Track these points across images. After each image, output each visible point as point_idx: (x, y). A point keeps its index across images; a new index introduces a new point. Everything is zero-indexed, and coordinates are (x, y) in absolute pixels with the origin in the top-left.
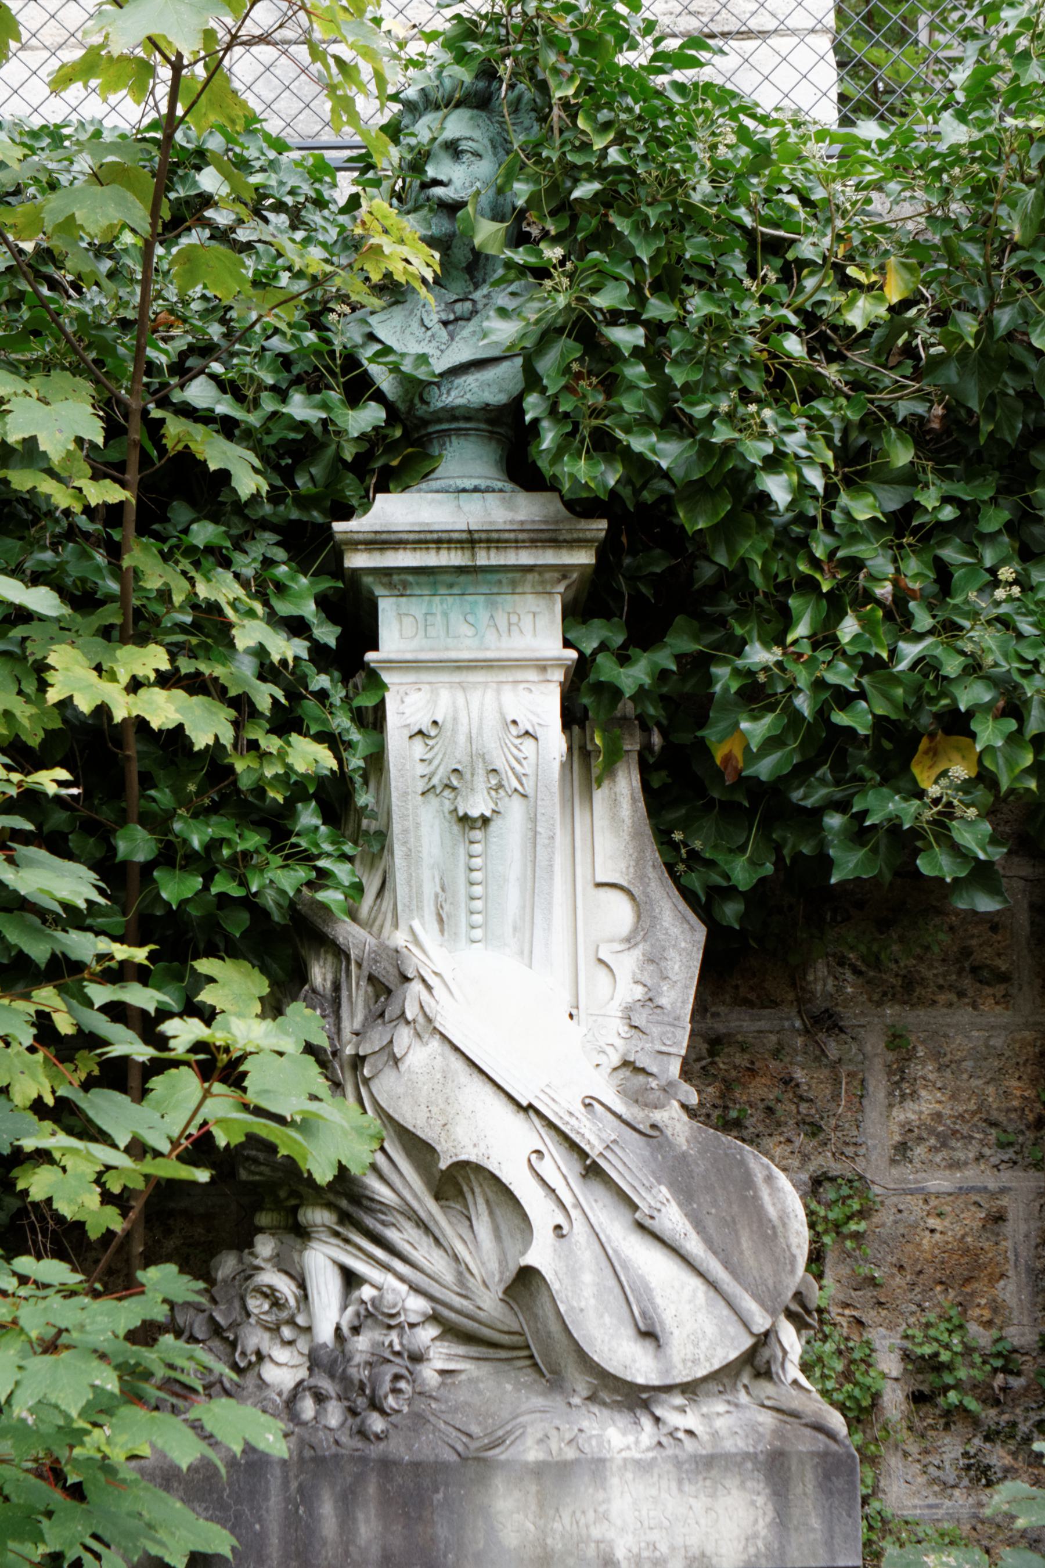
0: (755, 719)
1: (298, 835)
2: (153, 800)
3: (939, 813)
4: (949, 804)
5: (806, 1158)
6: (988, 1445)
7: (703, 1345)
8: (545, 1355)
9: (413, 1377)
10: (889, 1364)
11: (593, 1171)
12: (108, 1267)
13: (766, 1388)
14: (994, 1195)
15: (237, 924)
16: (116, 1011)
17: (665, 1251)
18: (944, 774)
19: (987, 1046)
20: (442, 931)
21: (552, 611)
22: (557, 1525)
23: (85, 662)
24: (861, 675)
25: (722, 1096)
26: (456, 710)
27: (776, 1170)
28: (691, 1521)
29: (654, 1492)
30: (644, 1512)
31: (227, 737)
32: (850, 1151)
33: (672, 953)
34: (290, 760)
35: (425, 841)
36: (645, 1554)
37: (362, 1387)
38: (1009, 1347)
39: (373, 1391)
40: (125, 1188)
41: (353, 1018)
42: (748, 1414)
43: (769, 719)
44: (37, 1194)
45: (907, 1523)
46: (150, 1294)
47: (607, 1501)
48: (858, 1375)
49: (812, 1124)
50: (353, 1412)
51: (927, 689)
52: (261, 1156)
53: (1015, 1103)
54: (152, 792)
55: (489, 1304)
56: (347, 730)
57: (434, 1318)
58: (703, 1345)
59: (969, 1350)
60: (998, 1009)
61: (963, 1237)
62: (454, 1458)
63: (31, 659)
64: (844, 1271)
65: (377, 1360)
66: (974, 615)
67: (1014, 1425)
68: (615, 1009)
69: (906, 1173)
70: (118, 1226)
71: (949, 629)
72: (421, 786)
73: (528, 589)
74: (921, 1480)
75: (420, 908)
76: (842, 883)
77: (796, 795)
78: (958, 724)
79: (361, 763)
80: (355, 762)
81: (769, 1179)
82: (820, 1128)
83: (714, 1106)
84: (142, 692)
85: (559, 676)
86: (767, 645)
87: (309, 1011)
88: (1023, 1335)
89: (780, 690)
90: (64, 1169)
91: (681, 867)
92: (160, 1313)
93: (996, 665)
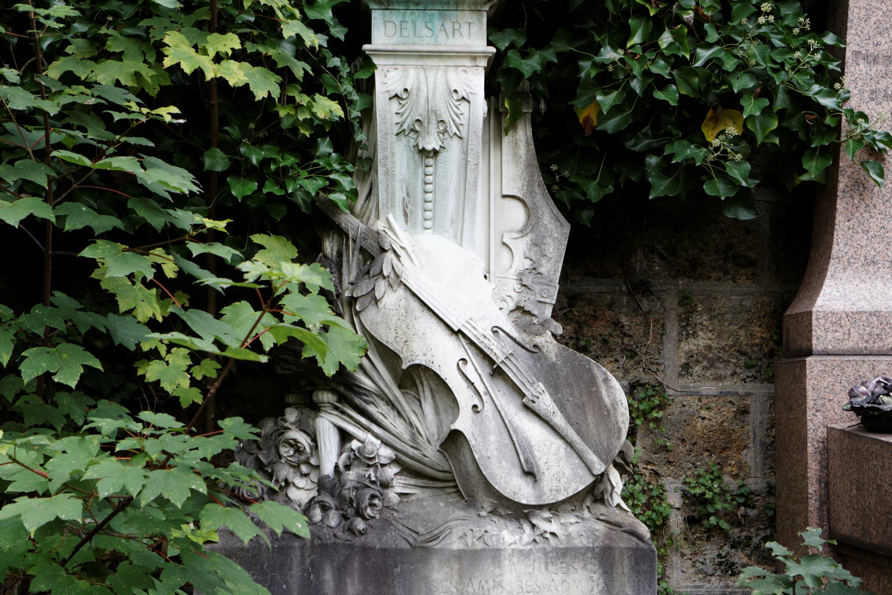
0: (606, 94)
1: (318, 158)
2: (227, 133)
3: (718, 157)
4: (725, 152)
5: (626, 372)
6: (733, 550)
7: (563, 481)
8: (465, 486)
10: (674, 499)
11: (497, 372)
12: (199, 421)
13: (601, 509)
15: (278, 214)
16: (204, 261)
17: (541, 422)
18: (722, 132)
19: (741, 305)
20: (406, 221)
21: (481, 22)
22: (470, 589)
23: (188, 43)
24: (672, 70)
25: (576, 332)
26: (419, 83)
27: (610, 375)
29: (530, 570)
30: (524, 582)
31: (276, 93)
32: (654, 368)
33: (549, 240)
34: (314, 110)
35: (397, 164)
37: (351, 500)
38: (748, 490)
39: (358, 504)
40: (204, 377)
41: (350, 274)
43: (614, 94)
44: (151, 377)
46: (226, 434)
47: (501, 575)
48: (654, 505)
49: (631, 351)
50: (345, 517)
51: (713, 79)
52: (291, 359)
53: (757, 341)
54: (227, 128)
55: (431, 453)
56: (350, 93)
57: (396, 461)
58: (563, 481)
59: (723, 492)
60: (748, 283)
61: (722, 422)
62: (408, 546)
63: (152, 41)
64: (648, 442)
65: (361, 486)
66: (744, 33)
67: (749, 538)
68: (512, 274)
69: (688, 382)
70: (199, 400)
71: (728, 42)
72: (396, 130)
73: (466, 8)
74: (692, 570)
75: (393, 207)
76: (656, 199)
77: (629, 144)
78: (732, 102)
79: (359, 114)
80: (355, 113)
81: (606, 380)
82: (636, 354)
83: (571, 338)
84: (223, 63)
85: (484, 63)
86: (614, 49)
87: (322, 269)
88: (757, 484)
89: (621, 77)
90: (167, 363)
91: (556, 187)
92: (233, 445)
93: (757, 64)
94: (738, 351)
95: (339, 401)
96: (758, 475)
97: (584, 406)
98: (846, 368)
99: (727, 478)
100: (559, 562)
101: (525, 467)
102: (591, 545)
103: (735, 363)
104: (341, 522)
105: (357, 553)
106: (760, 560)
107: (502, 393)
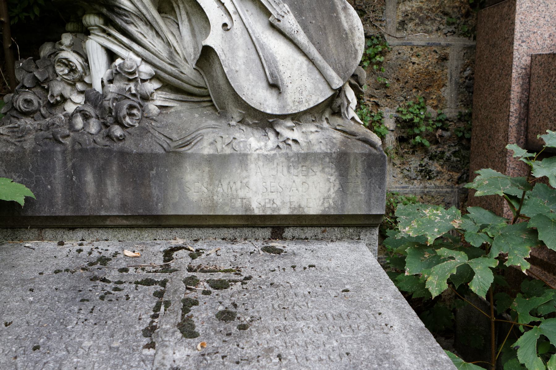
6: (431, 161)
8: (217, 99)
9: (142, 108)
13: (338, 121)
14: (444, 47)
17: (286, 40)
28: (294, 189)
29: (274, 172)
30: (268, 183)
36: (268, 206)
38: (445, 117)
42: (328, 133)
45: (393, 194)
47: (248, 177)
48: (375, 128)
53: (457, 4)
55: (188, 70)
57: (155, 77)
61: (428, 66)
62: (162, 151)
65: (120, 97)
67: (443, 153)
74: (400, 176)
81: (345, 9)
82: (365, 12)
88: (451, 112)
94: (442, 12)
95: (106, 24)
96: (452, 107)
97: (325, 28)
98: (550, 5)
99: (429, 108)
100: (300, 165)
101: (270, 80)
102: (329, 151)
103: (440, 21)
104: (101, 129)
105: (115, 156)
106: (450, 168)
107: (250, 13)
